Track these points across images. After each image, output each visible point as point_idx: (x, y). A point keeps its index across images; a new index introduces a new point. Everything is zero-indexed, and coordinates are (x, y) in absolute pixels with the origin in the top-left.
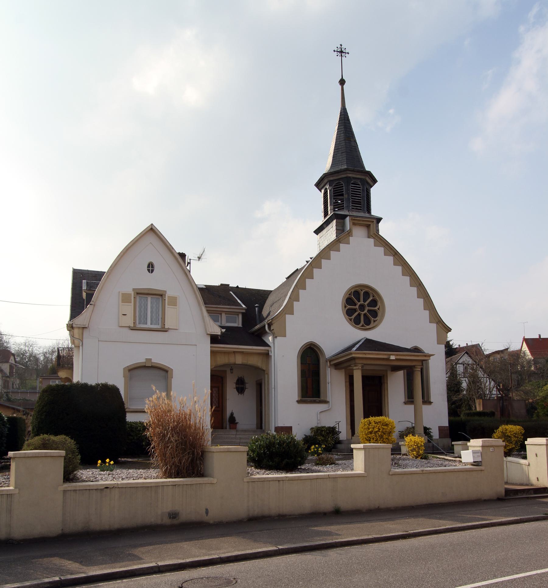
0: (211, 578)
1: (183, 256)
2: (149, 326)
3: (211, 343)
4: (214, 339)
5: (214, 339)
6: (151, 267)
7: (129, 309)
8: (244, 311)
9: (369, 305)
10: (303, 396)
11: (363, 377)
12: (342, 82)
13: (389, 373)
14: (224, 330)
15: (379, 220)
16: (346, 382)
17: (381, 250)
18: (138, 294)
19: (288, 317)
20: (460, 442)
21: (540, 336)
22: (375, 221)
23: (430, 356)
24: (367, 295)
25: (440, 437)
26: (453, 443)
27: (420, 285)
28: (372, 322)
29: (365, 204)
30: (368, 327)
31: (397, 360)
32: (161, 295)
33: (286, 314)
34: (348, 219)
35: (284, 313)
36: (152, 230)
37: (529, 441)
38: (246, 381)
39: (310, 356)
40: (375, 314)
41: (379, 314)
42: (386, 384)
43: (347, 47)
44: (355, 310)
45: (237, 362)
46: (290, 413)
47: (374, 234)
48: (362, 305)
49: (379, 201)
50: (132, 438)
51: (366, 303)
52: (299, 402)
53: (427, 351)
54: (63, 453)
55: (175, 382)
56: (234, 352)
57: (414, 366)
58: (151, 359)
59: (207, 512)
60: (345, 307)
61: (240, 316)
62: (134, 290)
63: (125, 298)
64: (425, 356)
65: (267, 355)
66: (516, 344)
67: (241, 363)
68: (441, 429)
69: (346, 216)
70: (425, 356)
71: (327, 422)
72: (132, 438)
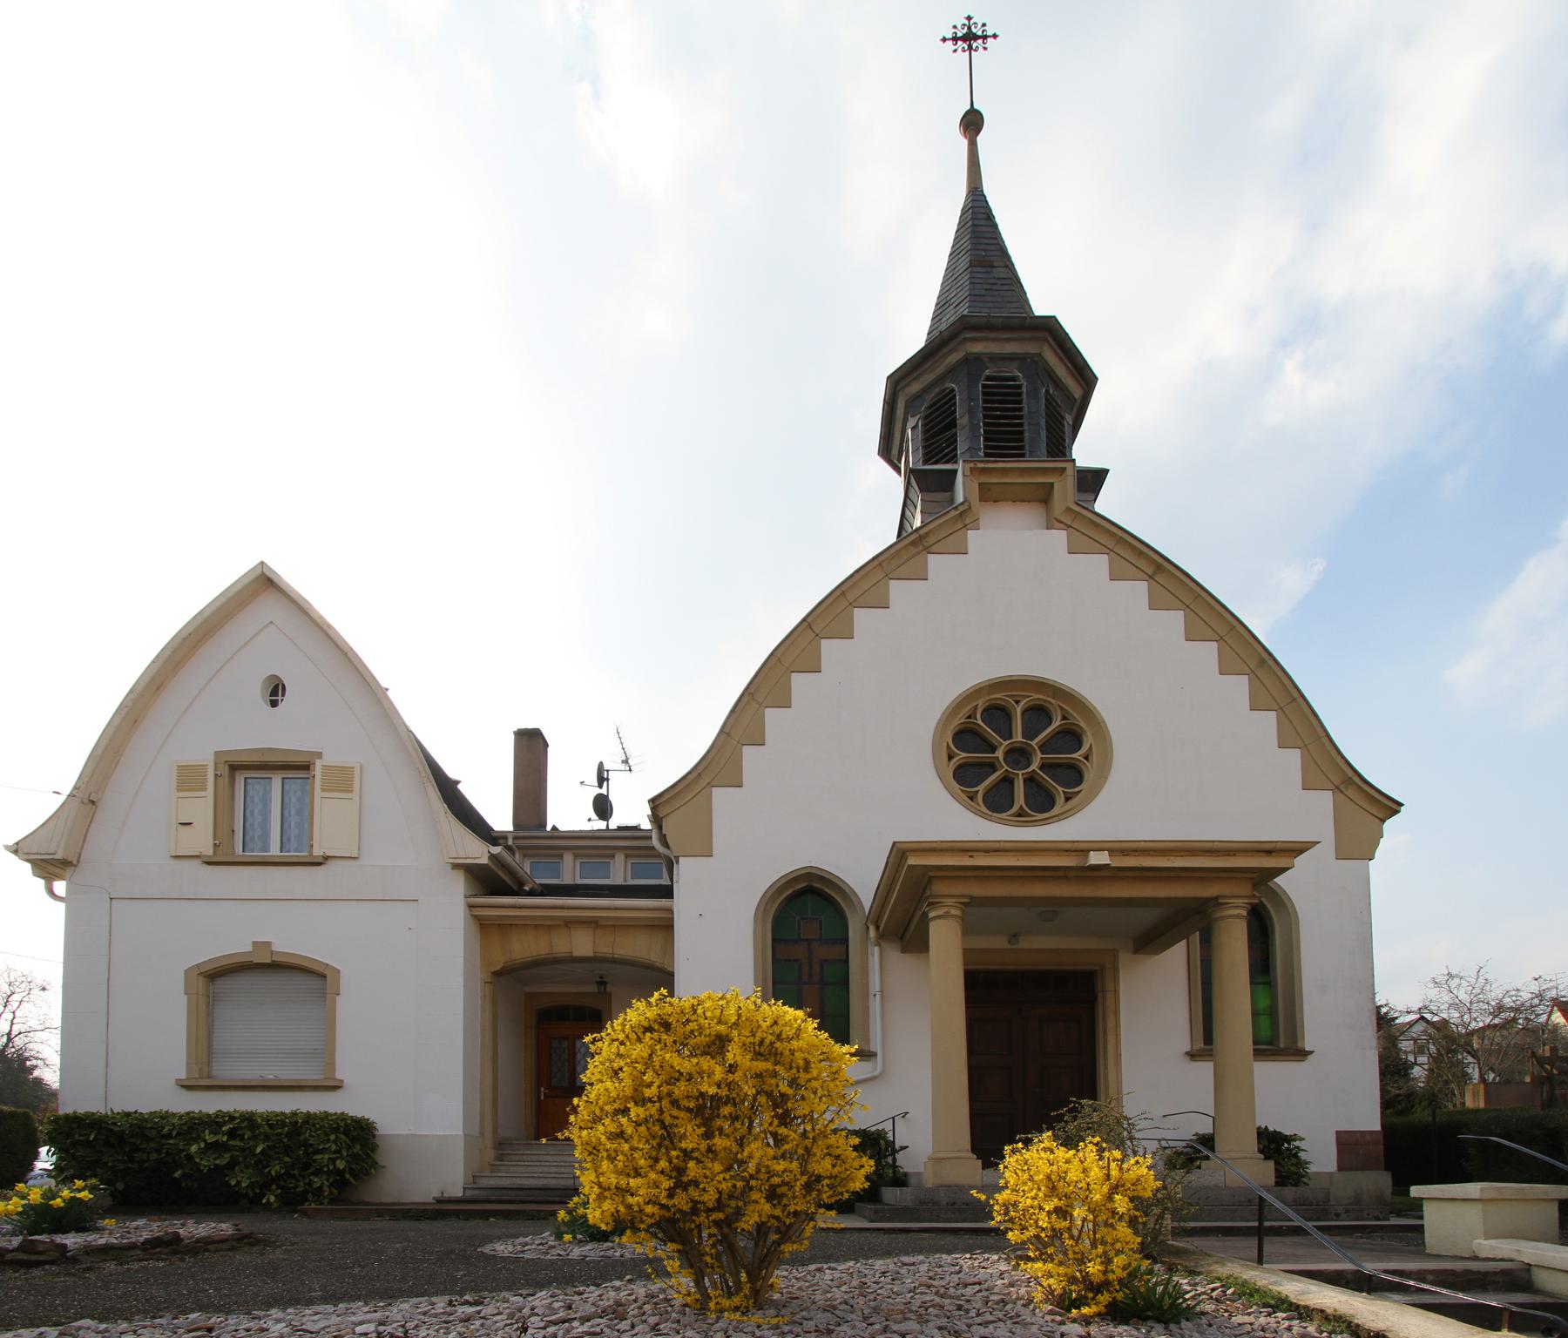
6: (276, 691)
7: (201, 808)
9: (1030, 733)
12: (972, 123)
13: (1125, 958)
18: (234, 768)
19: (718, 794)
20: (1473, 1189)
25: (1341, 1168)
26: (1416, 1191)
27: (1262, 662)
28: (1060, 799)
33: (710, 785)
35: (703, 783)
41: (1090, 774)
42: (1110, 996)
43: (954, 20)
45: (578, 952)
47: (1069, 509)
50: (1113, 1165)
55: (346, 1007)
56: (569, 924)
57: (1215, 902)
58: (268, 944)
60: (950, 758)
63: (188, 779)
65: (471, 906)
68: (1348, 1144)
72: (144, 1157)
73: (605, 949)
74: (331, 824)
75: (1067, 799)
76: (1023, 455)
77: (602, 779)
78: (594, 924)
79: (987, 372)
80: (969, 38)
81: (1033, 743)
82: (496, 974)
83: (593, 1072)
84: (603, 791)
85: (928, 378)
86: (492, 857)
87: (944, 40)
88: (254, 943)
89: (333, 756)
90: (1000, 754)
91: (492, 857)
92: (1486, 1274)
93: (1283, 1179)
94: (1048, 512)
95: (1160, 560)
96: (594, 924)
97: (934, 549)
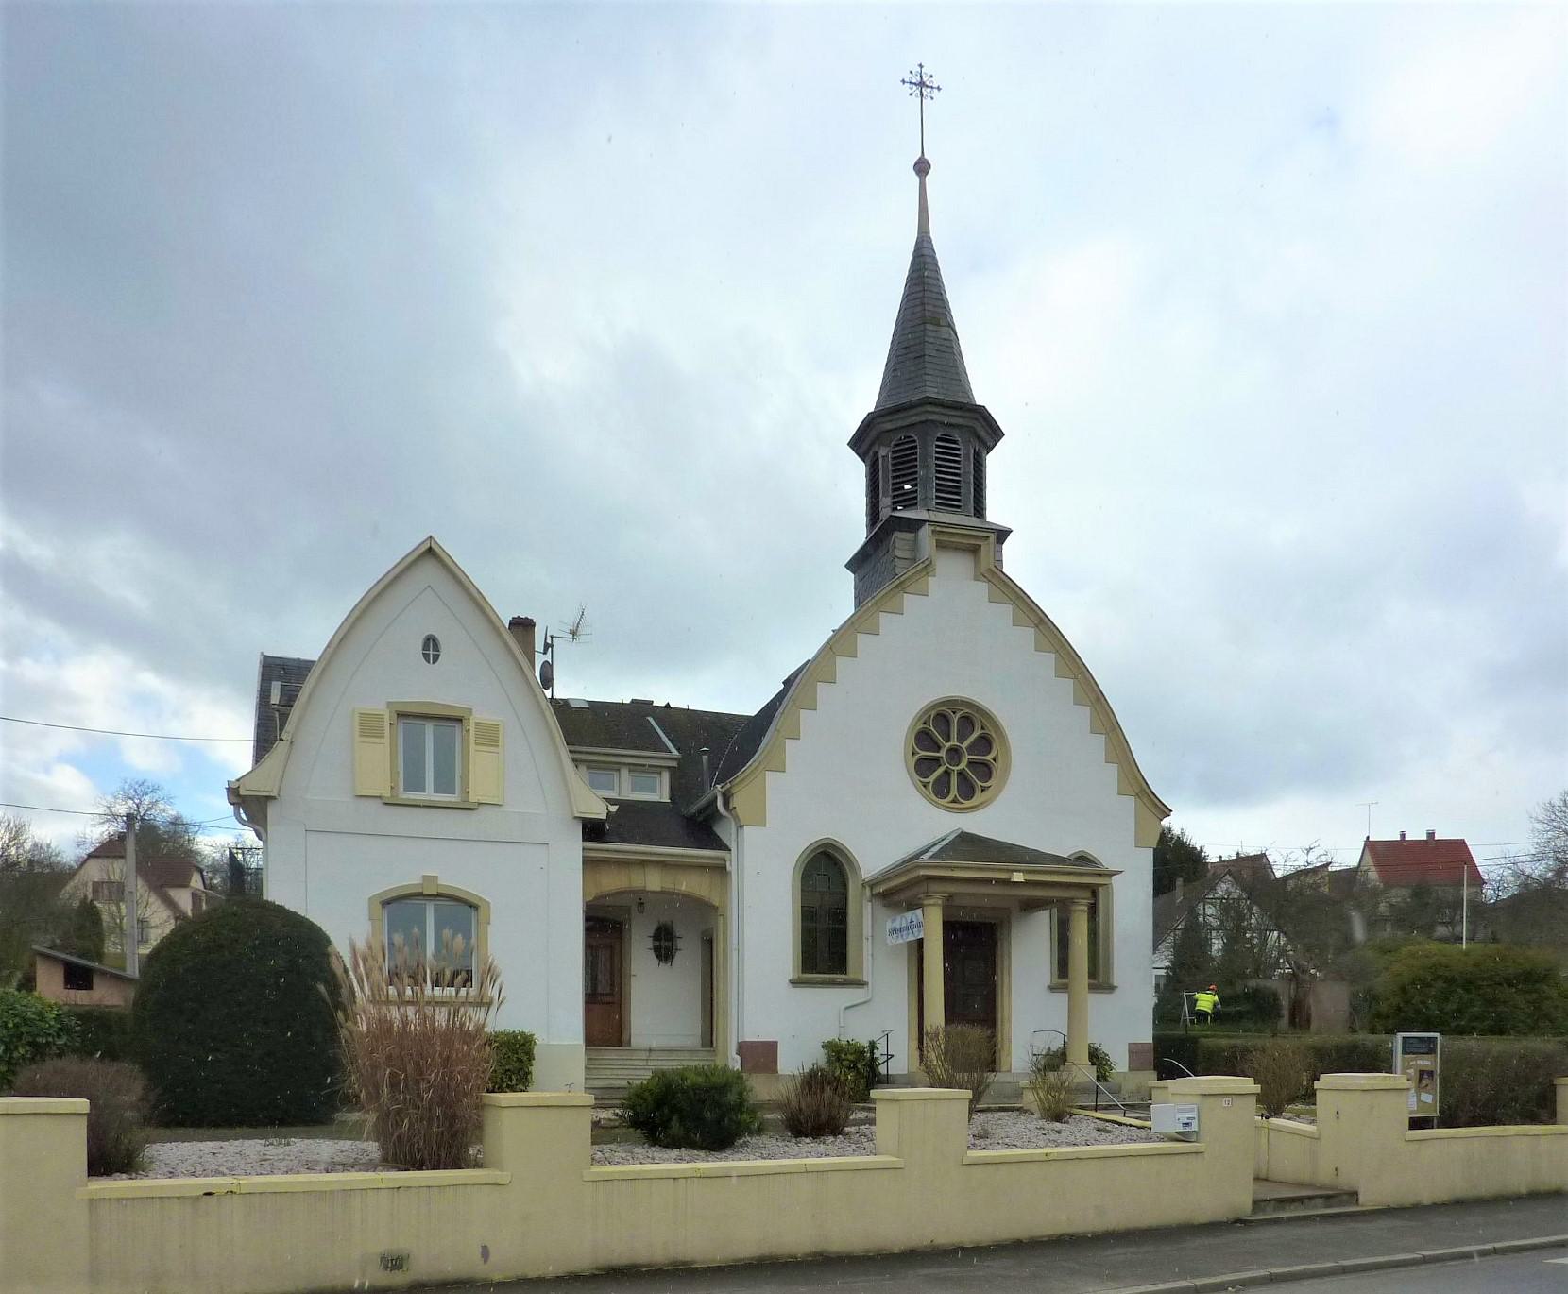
1: (523, 627)
2: (429, 795)
3: (584, 839)
4: (593, 830)
5: (593, 830)
6: (431, 648)
8: (675, 764)
9: (971, 749)
11: (949, 927)
12: (922, 167)
14: (614, 809)
15: (1002, 534)
17: (1006, 611)
18: (401, 715)
21: (1403, 835)
22: (992, 537)
23: (1111, 874)
24: (967, 722)
28: (978, 791)
29: (966, 489)
30: (967, 804)
31: (1027, 883)
32: (459, 720)
34: (925, 531)
36: (430, 553)
37: (1326, 1080)
38: (678, 931)
39: (825, 870)
40: (985, 770)
41: (997, 772)
43: (906, 67)
44: (937, 761)
46: (778, 1013)
48: (955, 749)
49: (1007, 486)
51: (964, 746)
52: (794, 983)
53: (1108, 863)
54: (82, 1104)
56: (643, 864)
59: (485, 1253)
61: (666, 776)
62: (389, 704)
63: (369, 726)
65: (720, 870)
66: (1348, 856)
68: (1135, 1050)
69: (921, 523)
71: (860, 1032)
73: (669, 886)
74: (483, 772)
78: (663, 865)
83: (140, 882)
88: (424, 877)
89: (480, 716)
90: (942, 753)
93: (1102, 1077)
94: (977, 562)
96: (663, 865)
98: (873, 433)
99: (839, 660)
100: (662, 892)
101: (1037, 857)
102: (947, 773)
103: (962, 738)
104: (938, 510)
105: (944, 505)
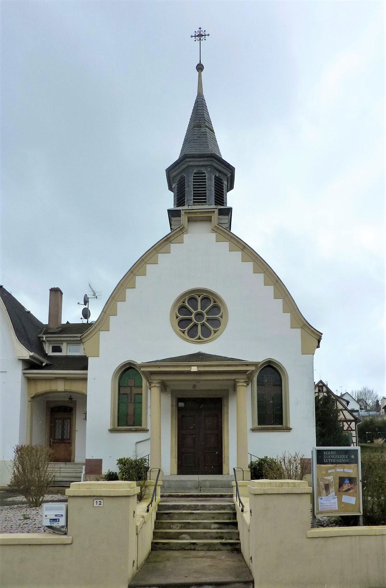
0: (325, 525)
10: (260, 422)
12: (200, 68)
16: (172, 406)
35: (97, 330)
39: (128, 373)
43: (194, 30)
45: (59, 390)
47: (215, 226)
48: (198, 312)
52: (112, 431)
56: (56, 379)
60: (177, 317)
64: (247, 365)
65: (24, 374)
67: (63, 390)
70: (247, 365)
75: (215, 332)
76: (205, 202)
77: (86, 302)
78: (65, 379)
79: (195, 171)
80: (200, 36)
81: (204, 312)
82: (33, 398)
84: (86, 307)
85: (177, 172)
86: (30, 356)
87: (192, 36)
91: (30, 356)
92: (225, 506)
95: (244, 244)
96: (65, 379)
97: (173, 242)
98: (171, 180)
99: (138, 278)
100: (65, 392)
101: (242, 360)
102: (203, 325)
103: (196, 308)
104: (194, 205)
105: (196, 202)
